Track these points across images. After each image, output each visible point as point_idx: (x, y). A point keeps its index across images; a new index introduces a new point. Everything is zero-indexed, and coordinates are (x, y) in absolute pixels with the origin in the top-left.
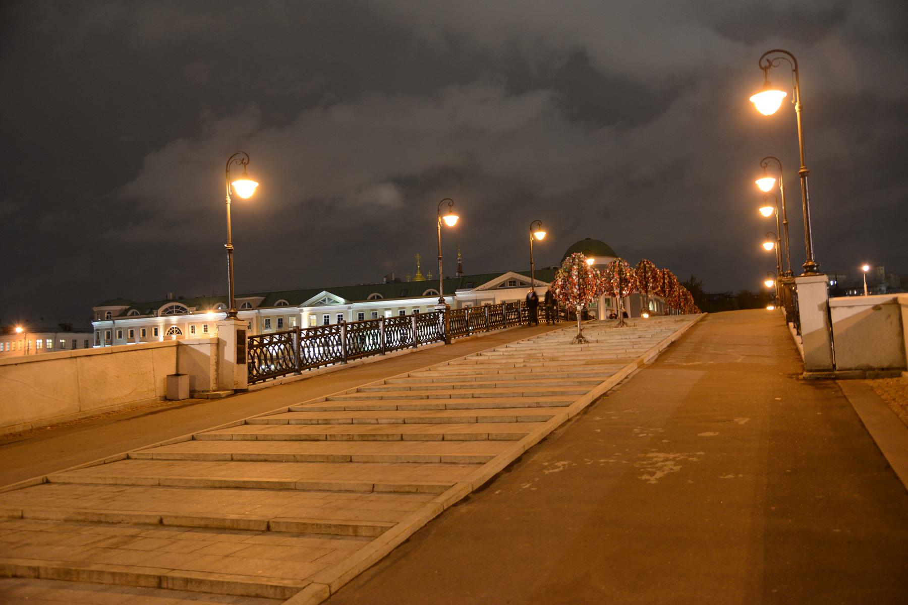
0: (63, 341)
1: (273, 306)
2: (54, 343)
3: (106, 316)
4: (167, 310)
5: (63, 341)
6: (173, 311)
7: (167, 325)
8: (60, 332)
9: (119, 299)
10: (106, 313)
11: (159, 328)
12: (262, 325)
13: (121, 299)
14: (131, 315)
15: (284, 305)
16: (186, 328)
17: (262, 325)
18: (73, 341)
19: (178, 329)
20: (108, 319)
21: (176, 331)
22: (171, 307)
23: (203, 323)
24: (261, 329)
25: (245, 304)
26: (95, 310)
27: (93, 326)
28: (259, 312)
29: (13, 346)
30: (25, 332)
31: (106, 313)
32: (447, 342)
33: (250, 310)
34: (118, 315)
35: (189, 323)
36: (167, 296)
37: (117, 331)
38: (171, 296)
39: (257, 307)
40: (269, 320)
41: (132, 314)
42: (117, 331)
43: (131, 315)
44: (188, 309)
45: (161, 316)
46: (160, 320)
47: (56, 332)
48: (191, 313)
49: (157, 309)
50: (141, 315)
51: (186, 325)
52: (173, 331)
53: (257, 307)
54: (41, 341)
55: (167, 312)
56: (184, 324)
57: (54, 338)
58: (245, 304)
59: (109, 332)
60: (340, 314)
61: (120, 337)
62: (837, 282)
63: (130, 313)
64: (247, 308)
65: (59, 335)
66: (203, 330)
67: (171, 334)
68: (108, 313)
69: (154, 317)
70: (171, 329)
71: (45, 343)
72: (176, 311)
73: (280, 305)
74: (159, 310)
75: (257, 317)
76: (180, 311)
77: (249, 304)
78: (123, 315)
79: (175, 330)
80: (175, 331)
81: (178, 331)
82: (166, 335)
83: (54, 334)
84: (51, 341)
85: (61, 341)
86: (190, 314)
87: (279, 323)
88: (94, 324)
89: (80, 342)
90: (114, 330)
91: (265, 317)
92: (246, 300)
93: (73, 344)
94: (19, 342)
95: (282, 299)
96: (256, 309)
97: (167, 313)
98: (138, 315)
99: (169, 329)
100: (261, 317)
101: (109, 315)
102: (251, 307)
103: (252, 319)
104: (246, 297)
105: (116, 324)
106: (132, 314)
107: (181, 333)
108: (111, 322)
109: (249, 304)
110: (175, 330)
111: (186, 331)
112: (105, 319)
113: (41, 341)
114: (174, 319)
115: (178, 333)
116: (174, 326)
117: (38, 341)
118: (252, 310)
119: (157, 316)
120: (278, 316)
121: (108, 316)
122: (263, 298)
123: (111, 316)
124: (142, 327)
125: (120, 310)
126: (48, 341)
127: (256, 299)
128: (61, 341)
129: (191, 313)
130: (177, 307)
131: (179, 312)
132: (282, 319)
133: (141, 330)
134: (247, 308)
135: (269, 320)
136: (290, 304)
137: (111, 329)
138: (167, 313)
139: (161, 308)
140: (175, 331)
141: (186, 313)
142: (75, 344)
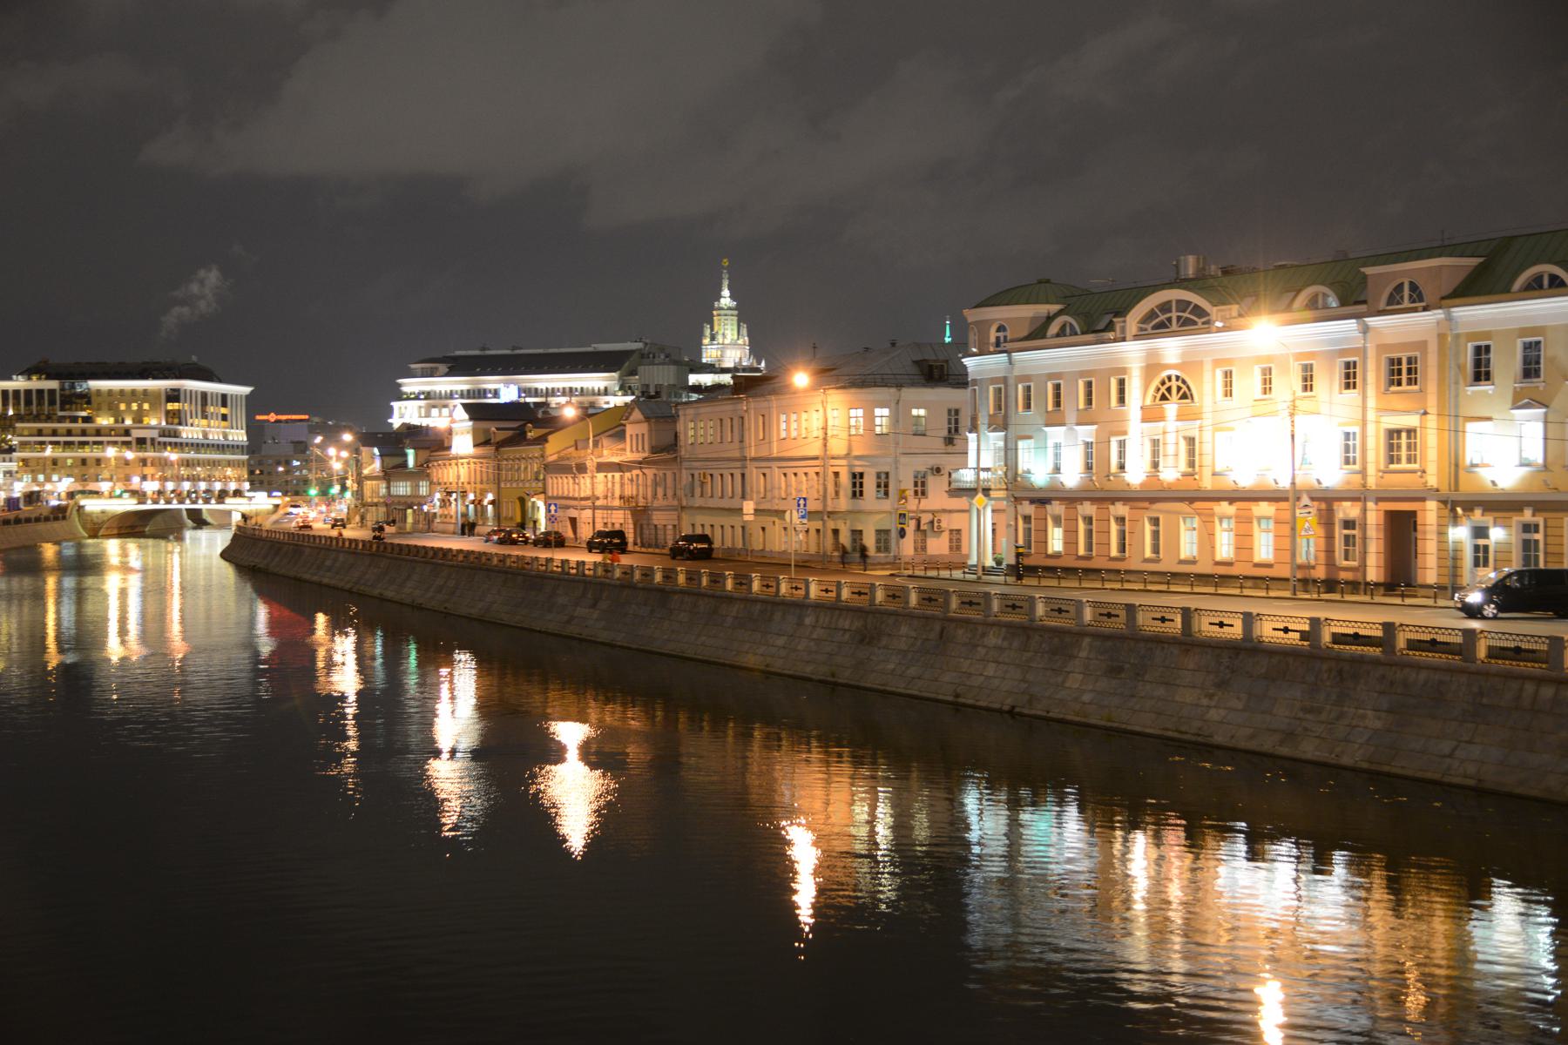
0: (922, 412)
1: (1508, 291)
2: (895, 419)
3: (993, 339)
4: (1151, 315)
5: (922, 412)
6: (1169, 320)
7: (1151, 368)
8: (913, 384)
9: (1040, 282)
10: (993, 330)
11: (1130, 378)
12: (1461, 368)
13: (1048, 281)
14: (1058, 335)
15: (1551, 285)
16: (1207, 376)
17: (1461, 368)
18: (949, 411)
19: (1184, 382)
20: (999, 347)
21: (1179, 389)
22: (1165, 307)
23: (1258, 359)
24: (1457, 383)
25: (1400, 287)
26: (970, 320)
27: (965, 367)
28: (1449, 319)
29: (804, 424)
30: (815, 387)
31: (993, 330)
32: (1020, 577)
33: (1415, 310)
34: (1025, 333)
35: (1217, 363)
36: (1177, 267)
37: (1020, 386)
38: (1190, 266)
39: (1443, 298)
40: (1488, 348)
41: (1061, 333)
42: (1020, 386)
43: (1058, 335)
44: (1213, 311)
45: (1137, 337)
46: (1131, 353)
47: (899, 386)
48: (1218, 324)
49: (1122, 312)
50: (1083, 333)
51: (1208, 367)
52: (1169, 390)
53: (1443, 298)
54: (860, 412)
55: (1158, 325)
56: (1201, 363)
57: (893, 405)
58: (1400, 287)
59: (1000, 389)
60: (1483, 343)
61: (1028, 406)
62: (330, 426)
63: (1054, 328)
64: (1406, 304)
65: (909, 393)
66: (1259, 386)
67: (1164, 398)
68: (999, 330)
69: (1115, 341)
70: (1163, 383)
71: (870, 418)
72: (1179, 318)
73: (1535, 288)
74: (1129, 318)
75: (1441, 337)
76: (1191, 320)
77: (1414, 287)
78: (1037, 335)
79: (1174, 384)
80: (1174, 390)
81: (1184, 388)
82: (1148, 402)
83: (893, 390)
84: (886, 412)
85: (915, 412)
86: (1219, 330)
87: (1527, 361)
88: (966, 361)
89: (7, 459)
90: (1011, 382)
91: (1471, 336)
92: (1404, 273)
93: (950, 423)
94: (815, 415)
95: (1549, 262)
96: (1440, 308)
97: (1154, 328)
98: (1076, 334)
99: (1156, 382)
100: (1457, 336)
101: (1001, 334)
102: (1421, 300)
103: (1422, 346)
104: (1418, 258)
105: (1017, 365)
106: (1061, 333)
107: (1192, 399)
108: (1003, 357)
109: (1414, 287)
110: (1174, 384)
111: (1207, 387)
112: (992, 349)
113: (860, 412)
114: (1171, 348)
115: (1184, 397)
116: (1173, 373)
117: (853, 413)
118: (1425, 309)
119: (1124, 340)
120: (1523, 332)
121: (998, 338)
122: (1475, 261)
123: (1005, 337)
124: (1082, 374)
125: (1033, 319)
126: (878, 412)
127: (1440, 267)
128: (915, 412)
129: (1218, 324)
130: (1183, 305)
131: (1188, 322)
132: (1538, 343)
133: (1081, 384)
134: (1406, 304)
135: (1488, 348)
136: (1344, 302)
137: (1005, 380)
138: (1154, 328)
139: (1142, 303)
140: (1174, 390)
141: (1207, 327)
142: (957, 421)
